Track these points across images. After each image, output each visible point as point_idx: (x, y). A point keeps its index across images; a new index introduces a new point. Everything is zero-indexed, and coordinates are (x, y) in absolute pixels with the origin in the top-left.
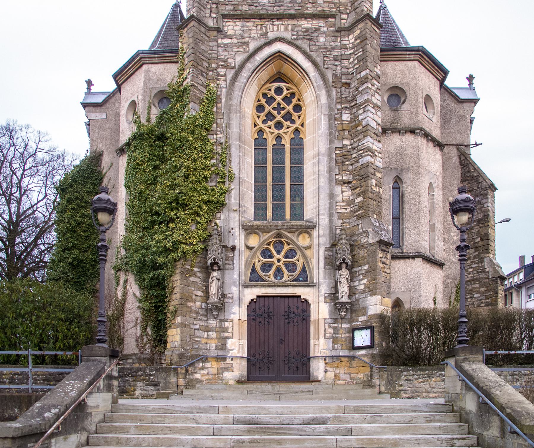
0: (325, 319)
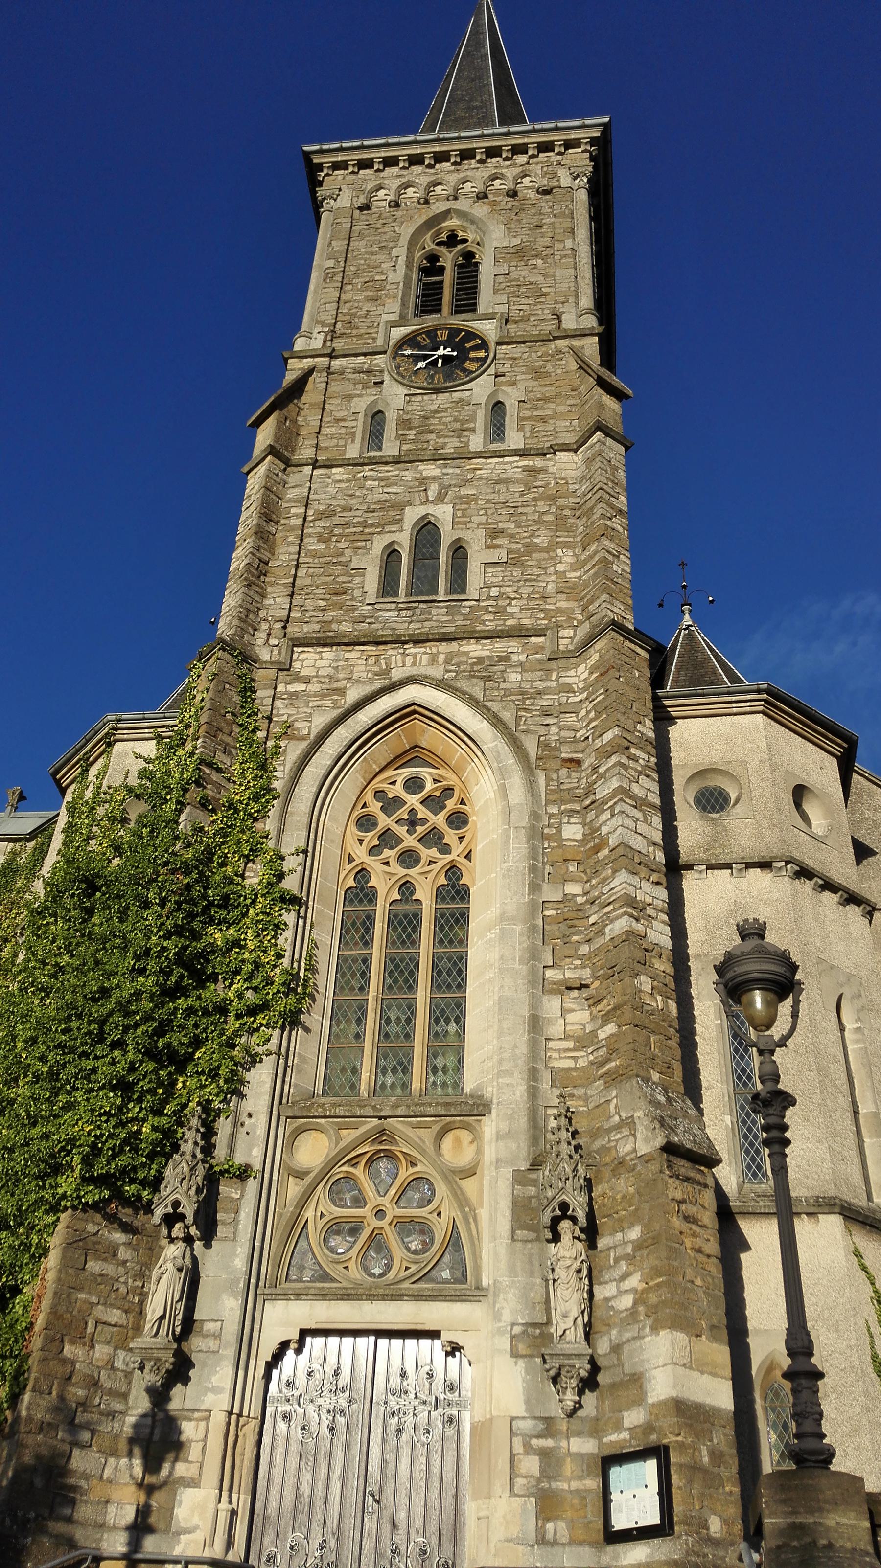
0: (512, 1419)
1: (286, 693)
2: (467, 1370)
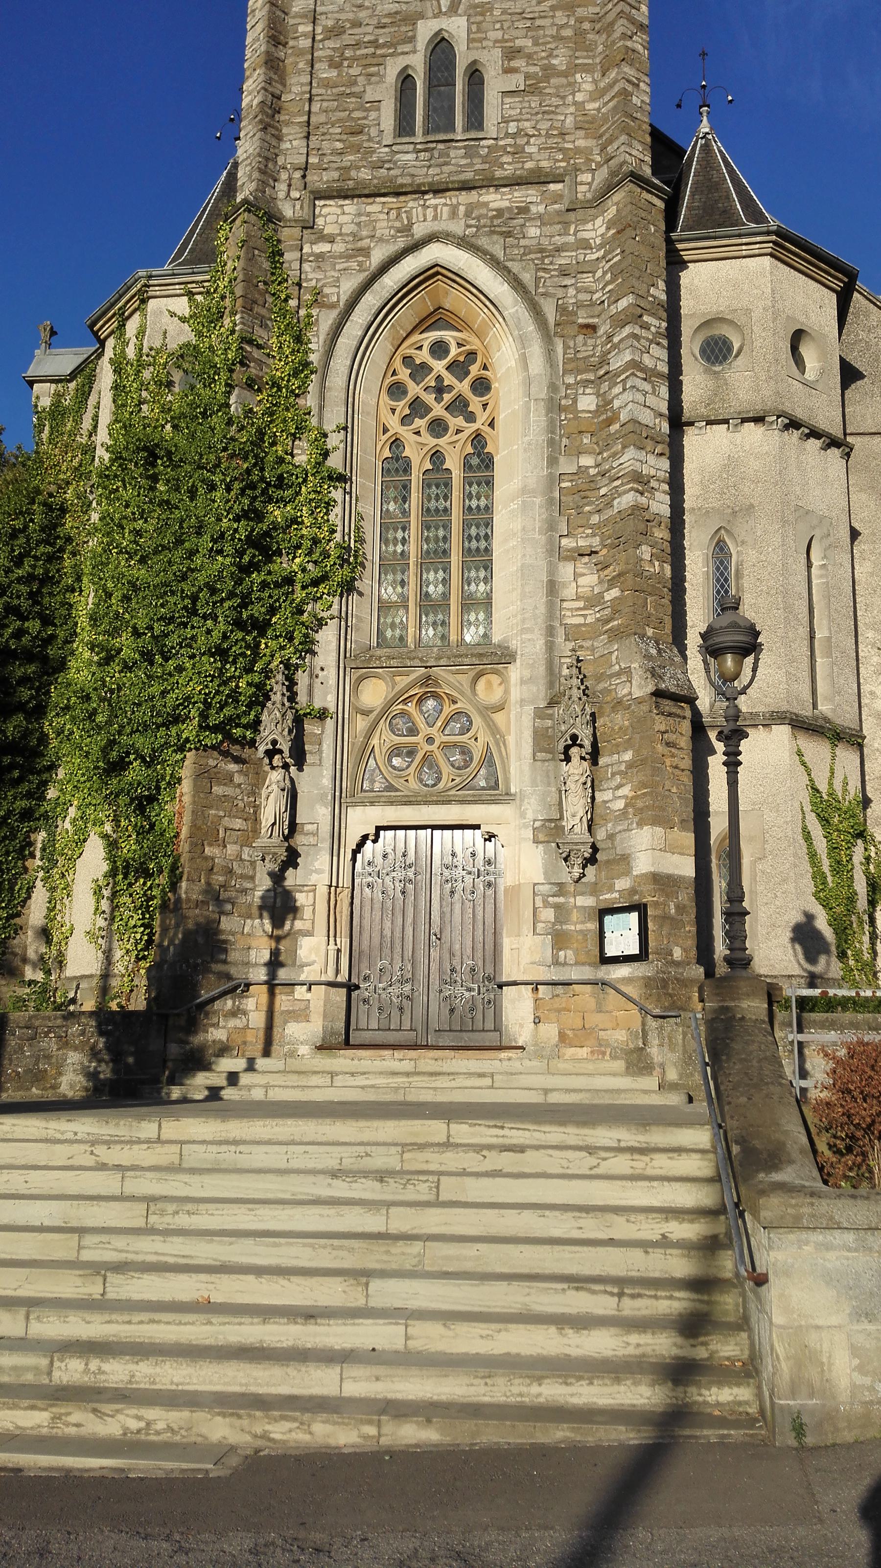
0: (535, 884)
1: (312, 254)
2: (501, 852)
